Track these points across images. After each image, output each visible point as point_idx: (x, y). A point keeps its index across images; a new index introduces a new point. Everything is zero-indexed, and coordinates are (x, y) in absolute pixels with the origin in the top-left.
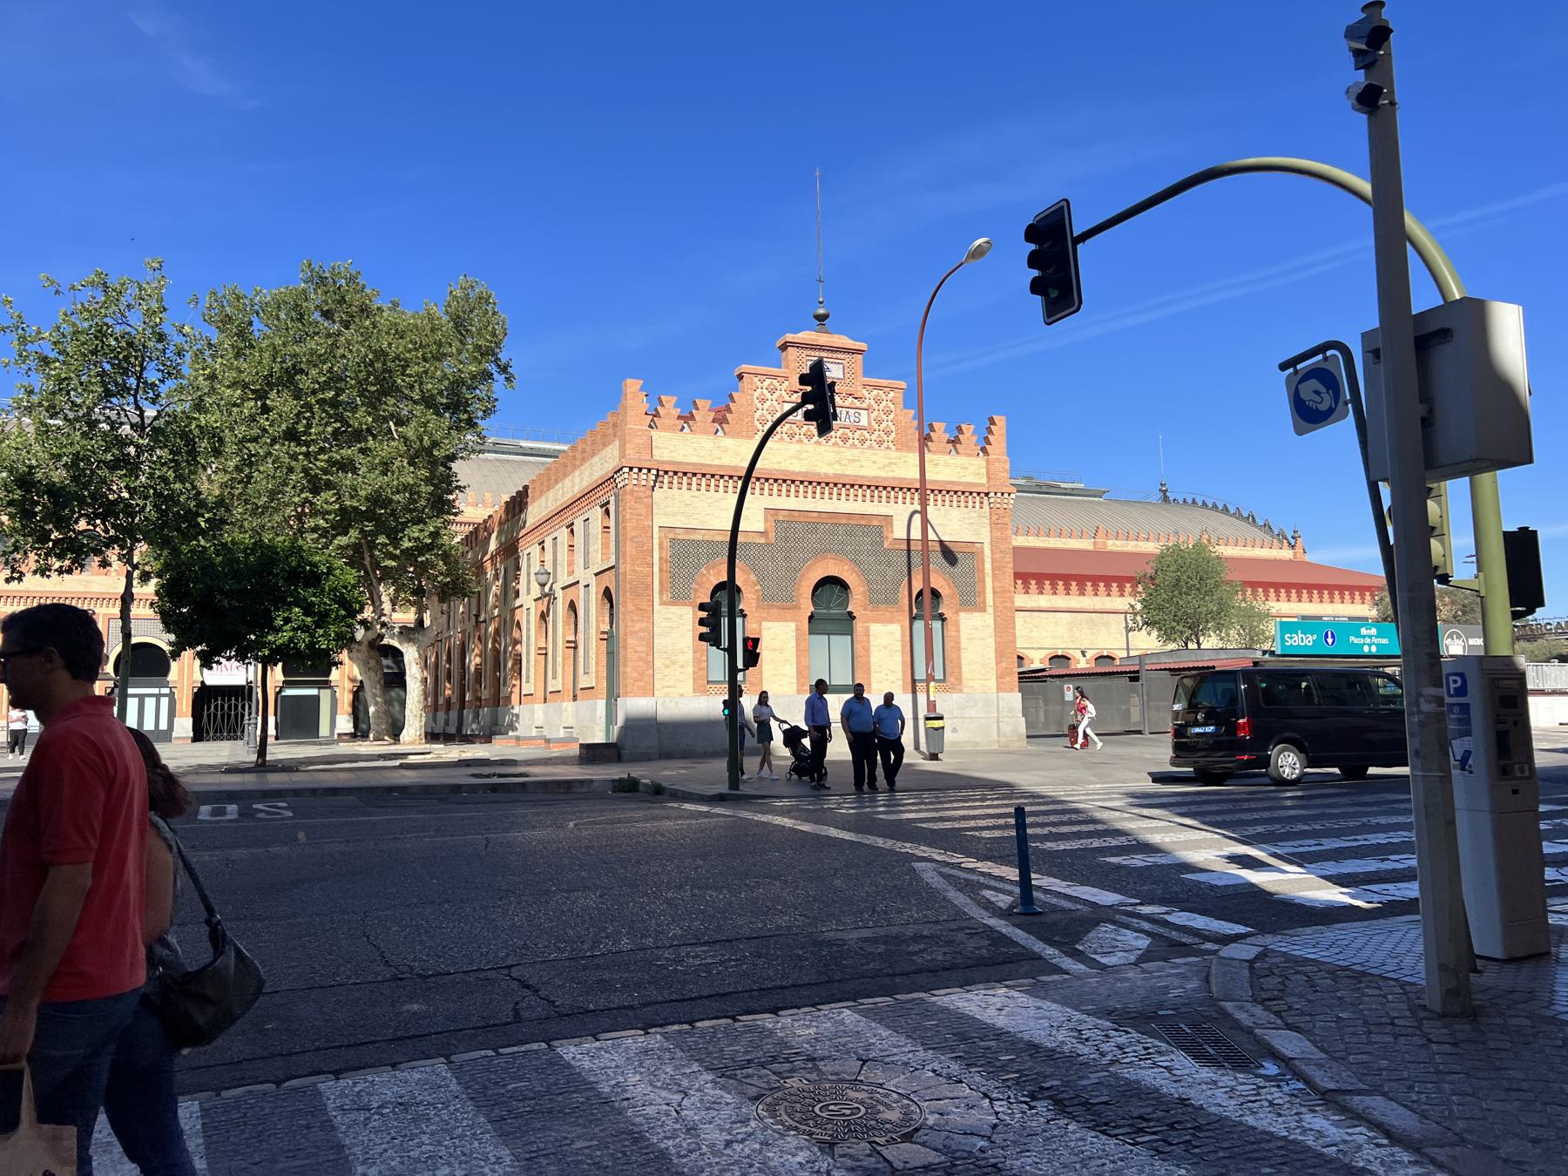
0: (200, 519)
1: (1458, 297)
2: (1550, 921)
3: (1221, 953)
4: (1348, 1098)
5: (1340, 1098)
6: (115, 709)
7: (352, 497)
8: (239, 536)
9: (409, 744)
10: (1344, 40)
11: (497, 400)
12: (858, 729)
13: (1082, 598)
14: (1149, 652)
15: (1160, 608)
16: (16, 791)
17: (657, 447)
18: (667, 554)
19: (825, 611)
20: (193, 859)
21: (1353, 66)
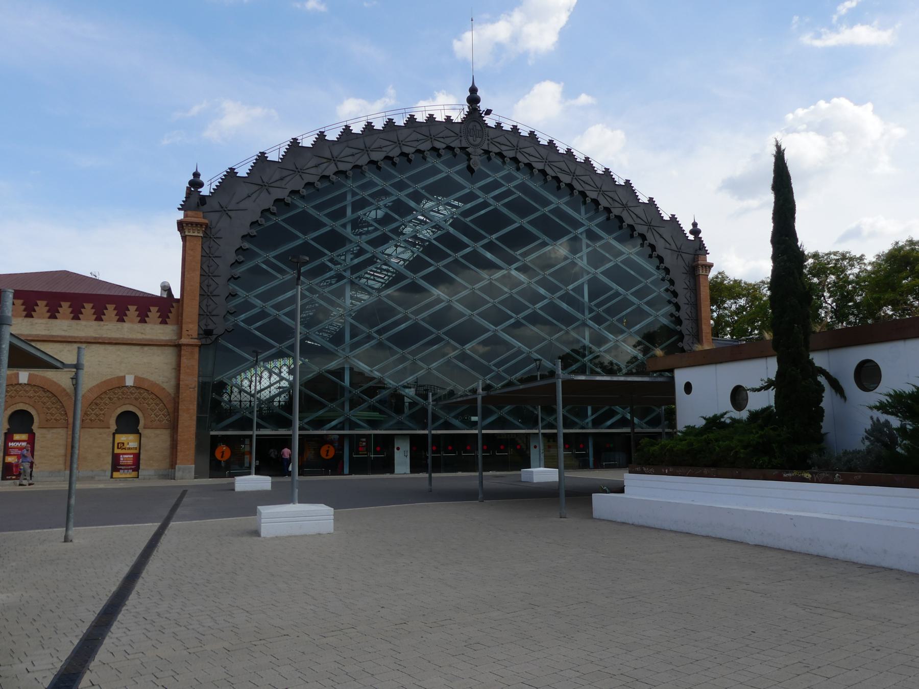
1: (478, 482)
6: (382, 419)
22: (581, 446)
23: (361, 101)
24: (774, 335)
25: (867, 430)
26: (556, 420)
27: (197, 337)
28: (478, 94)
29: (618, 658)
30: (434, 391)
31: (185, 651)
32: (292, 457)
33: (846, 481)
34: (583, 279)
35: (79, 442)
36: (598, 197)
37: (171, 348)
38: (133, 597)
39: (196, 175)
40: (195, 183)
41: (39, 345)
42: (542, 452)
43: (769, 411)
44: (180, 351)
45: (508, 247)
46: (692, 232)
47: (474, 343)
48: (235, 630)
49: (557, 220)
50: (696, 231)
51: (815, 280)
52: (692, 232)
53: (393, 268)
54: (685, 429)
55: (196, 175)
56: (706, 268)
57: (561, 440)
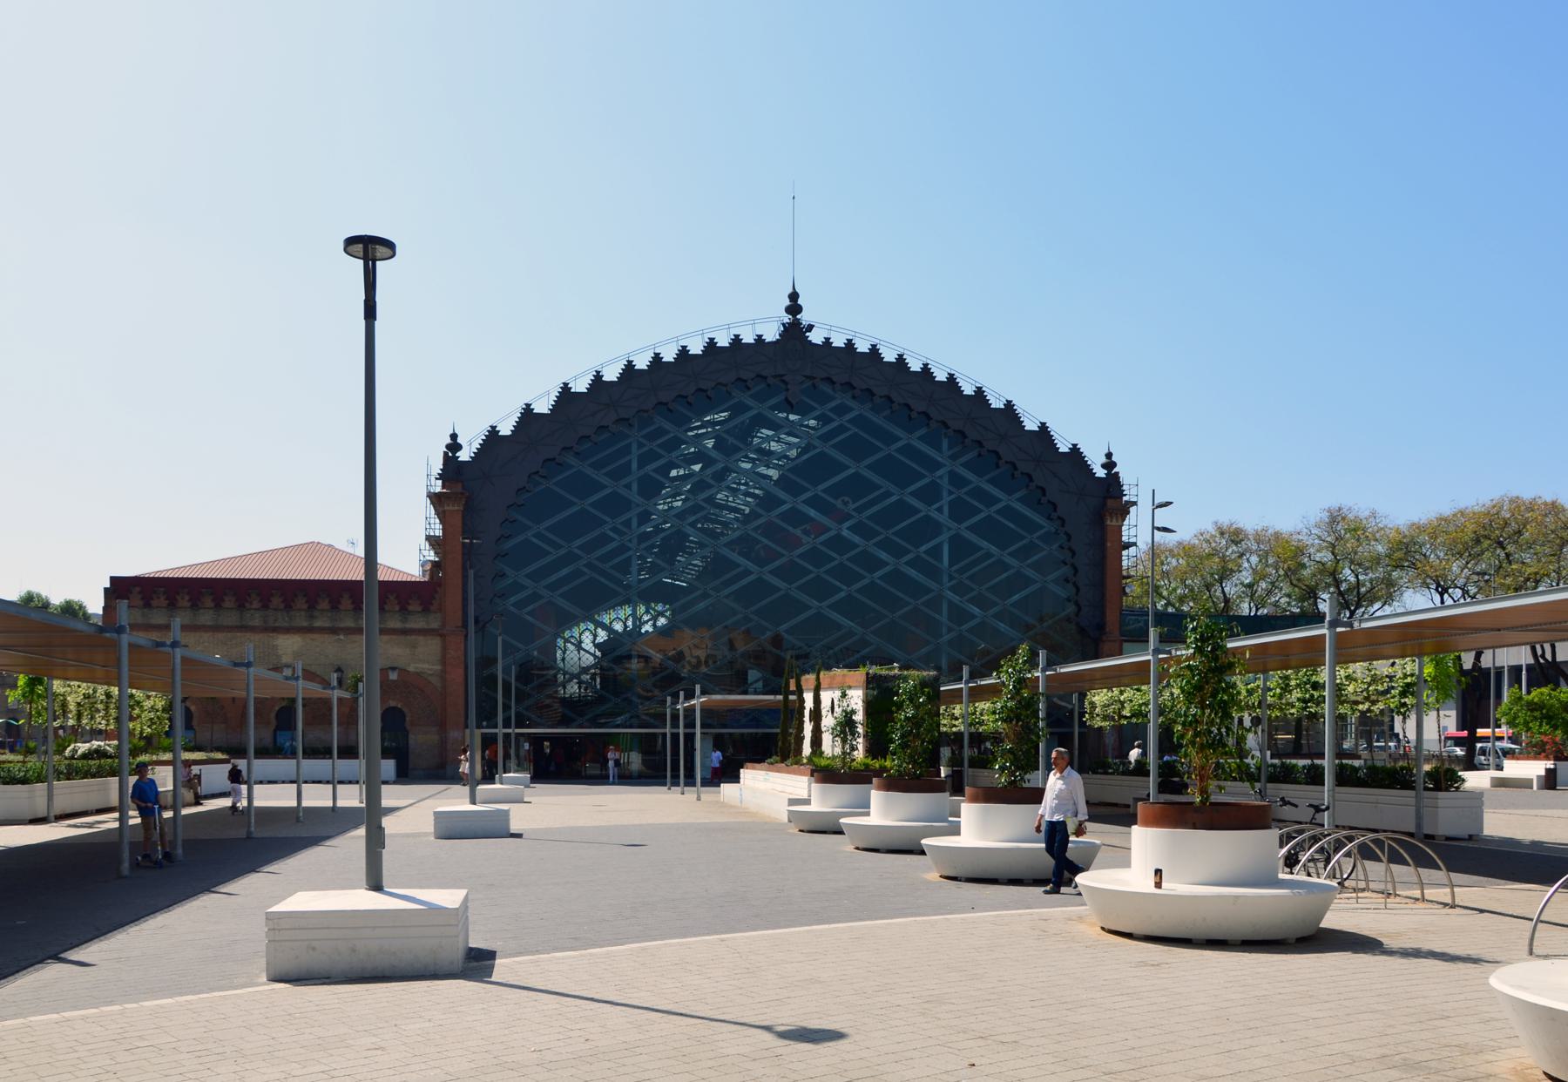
19: (861, 433)
21: (1539, 774)
28: (1113, 459)
34: (861, 433)
39: (454, 436)
40: (454, 446)
46: (1104, 466)
50: (1110, 465)
52: (1104, 466)
55: (454, 436)
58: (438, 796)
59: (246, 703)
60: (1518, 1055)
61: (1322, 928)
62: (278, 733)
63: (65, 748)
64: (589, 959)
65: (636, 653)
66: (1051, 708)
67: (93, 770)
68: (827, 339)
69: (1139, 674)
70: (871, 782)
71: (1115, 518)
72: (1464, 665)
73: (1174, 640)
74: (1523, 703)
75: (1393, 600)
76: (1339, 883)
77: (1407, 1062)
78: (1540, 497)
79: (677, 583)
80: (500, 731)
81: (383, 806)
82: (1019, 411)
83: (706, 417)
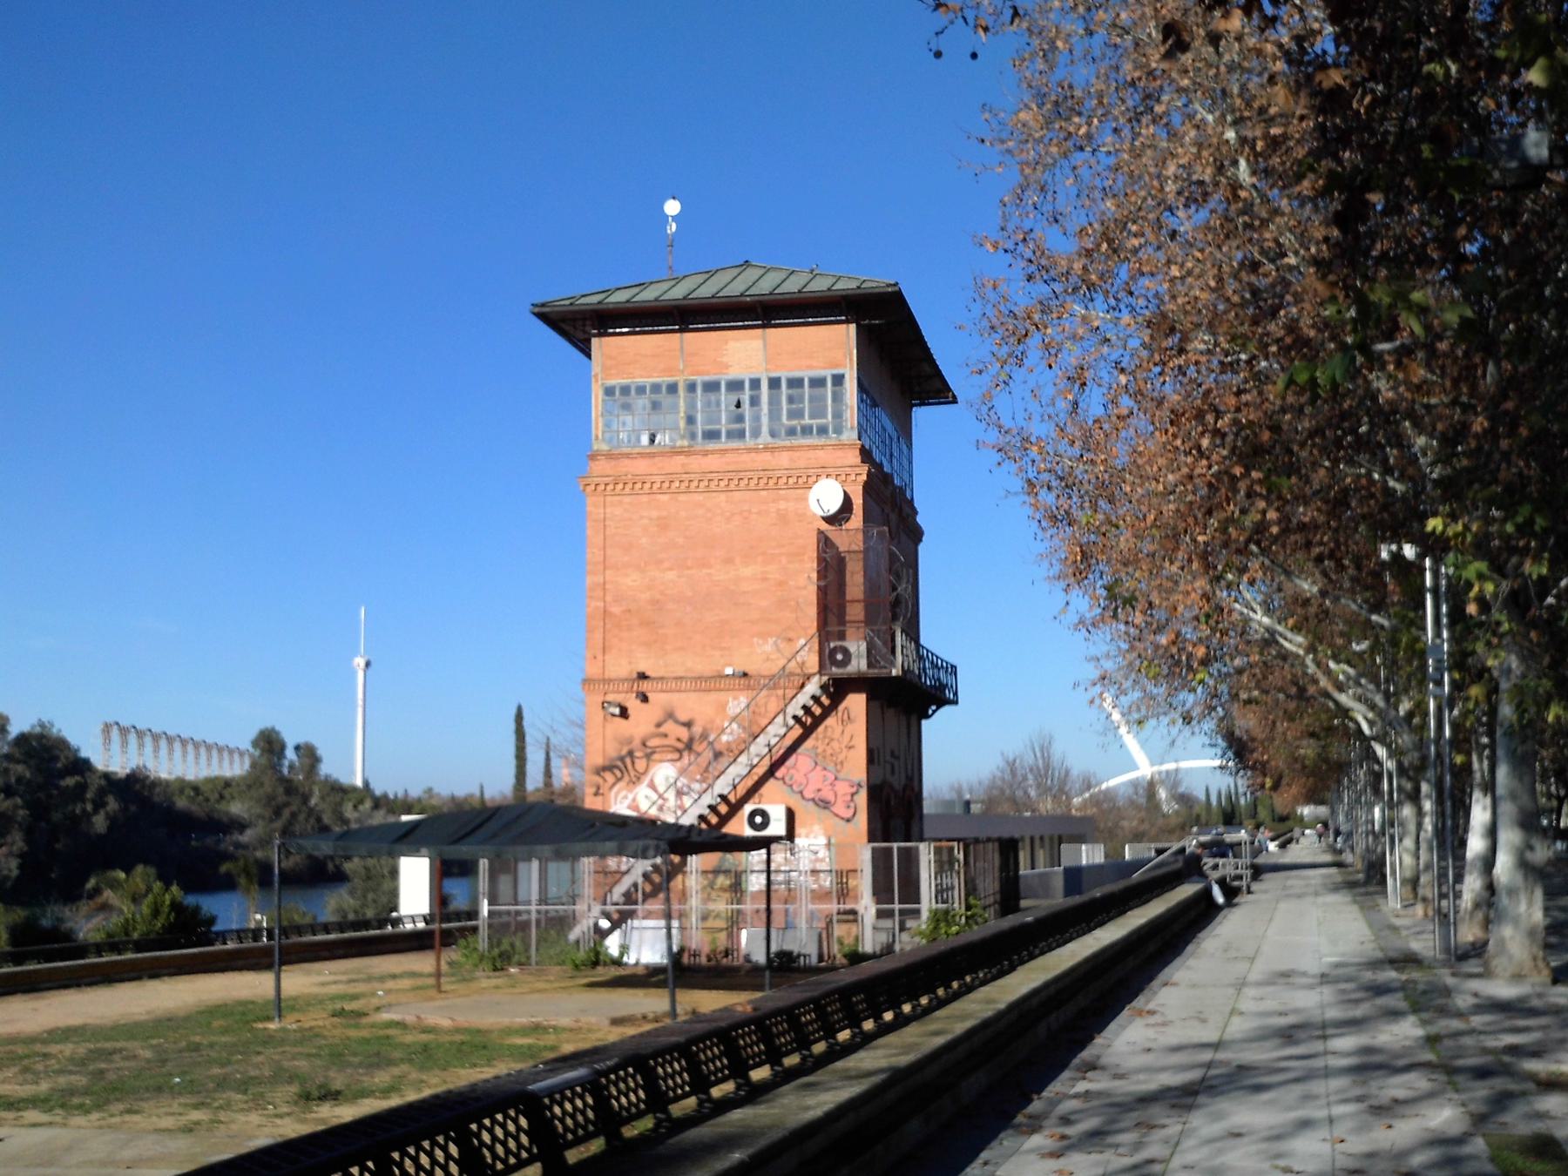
0: (1383, 547)
2: (585, 860)
3: (817, 677)
4: (679, 443)
5: (707, 276)
6: (1444, 609)
7: (262, 785)
8: (1123, 460)
9: (99, 949)
10: (253, 733)
11: (1030, 278)
12: (446, 857)
13: (801, 704)
14: (32, 1115)
15: (1186, 313)
16: (1063, 1066)
17: (778, 871)
18: (562, 913)
19: (378, 932)
20: (555, 762)
22: (70, 781)
23: (1312, 807)
24: (1464, 610)
25: (1237, 733)
26: (890, 559)
27: (284, 994)
29: (1090, 224)
30: (1172, 349)
31: (1169, 1018)
32: (1047, 1151)
33: (91, 984)
34: (378, 932)
35: (555, 989)
36: (858, 601)
37: (283, 975)
38: (820, 285)
41: (721, 294)
42: (1445, 620)
43: (210, 841)
44: (786, 922)
45: (83, 958)
47: (1138, 1082)
48: (1282, 1163)
49: (158, 954)
51: (1407, 181)
53: (896, 1048)
54: (1302, 95)
56: (171, 751)
57: (897, 913)
58: (478, 821)
59: (1545, 1052)
60: (820, 453)
61: (726, 835)
62: (996, 844)
63: (1360, 730)
64: (1307, 886)
65: (1471, 1001)
66: (1176, 549)
67: (117, 1057)
68: (270, 743)
69: (1438, 634)
70: (845, 956)
71: (227, 843)
72: (761, 346)
73: (126, 976)
74: (1554, 591)
75: (968, 804)
76: (1198, 816)
77: (1298, 1089)
78: (1187, 719)
79: (1428, 596)
80: (533, 908)
81: (1102, 860)
82: (400, 795)
83: (1392, 576)
